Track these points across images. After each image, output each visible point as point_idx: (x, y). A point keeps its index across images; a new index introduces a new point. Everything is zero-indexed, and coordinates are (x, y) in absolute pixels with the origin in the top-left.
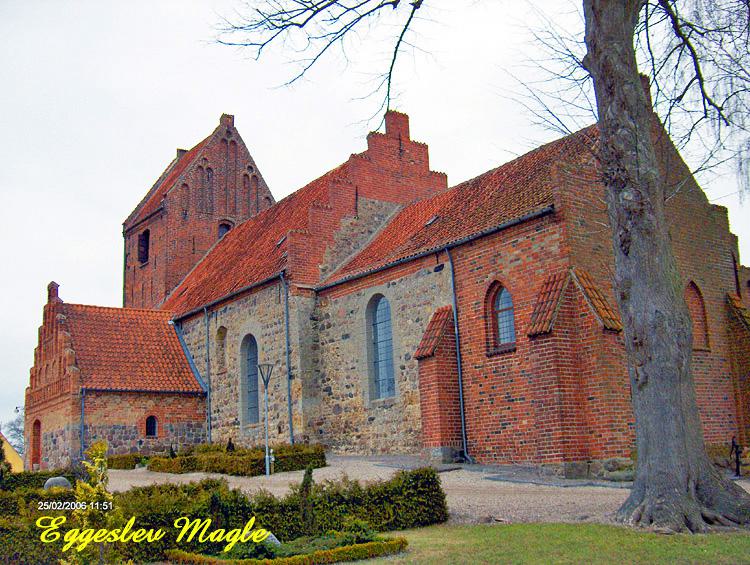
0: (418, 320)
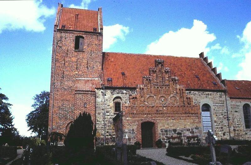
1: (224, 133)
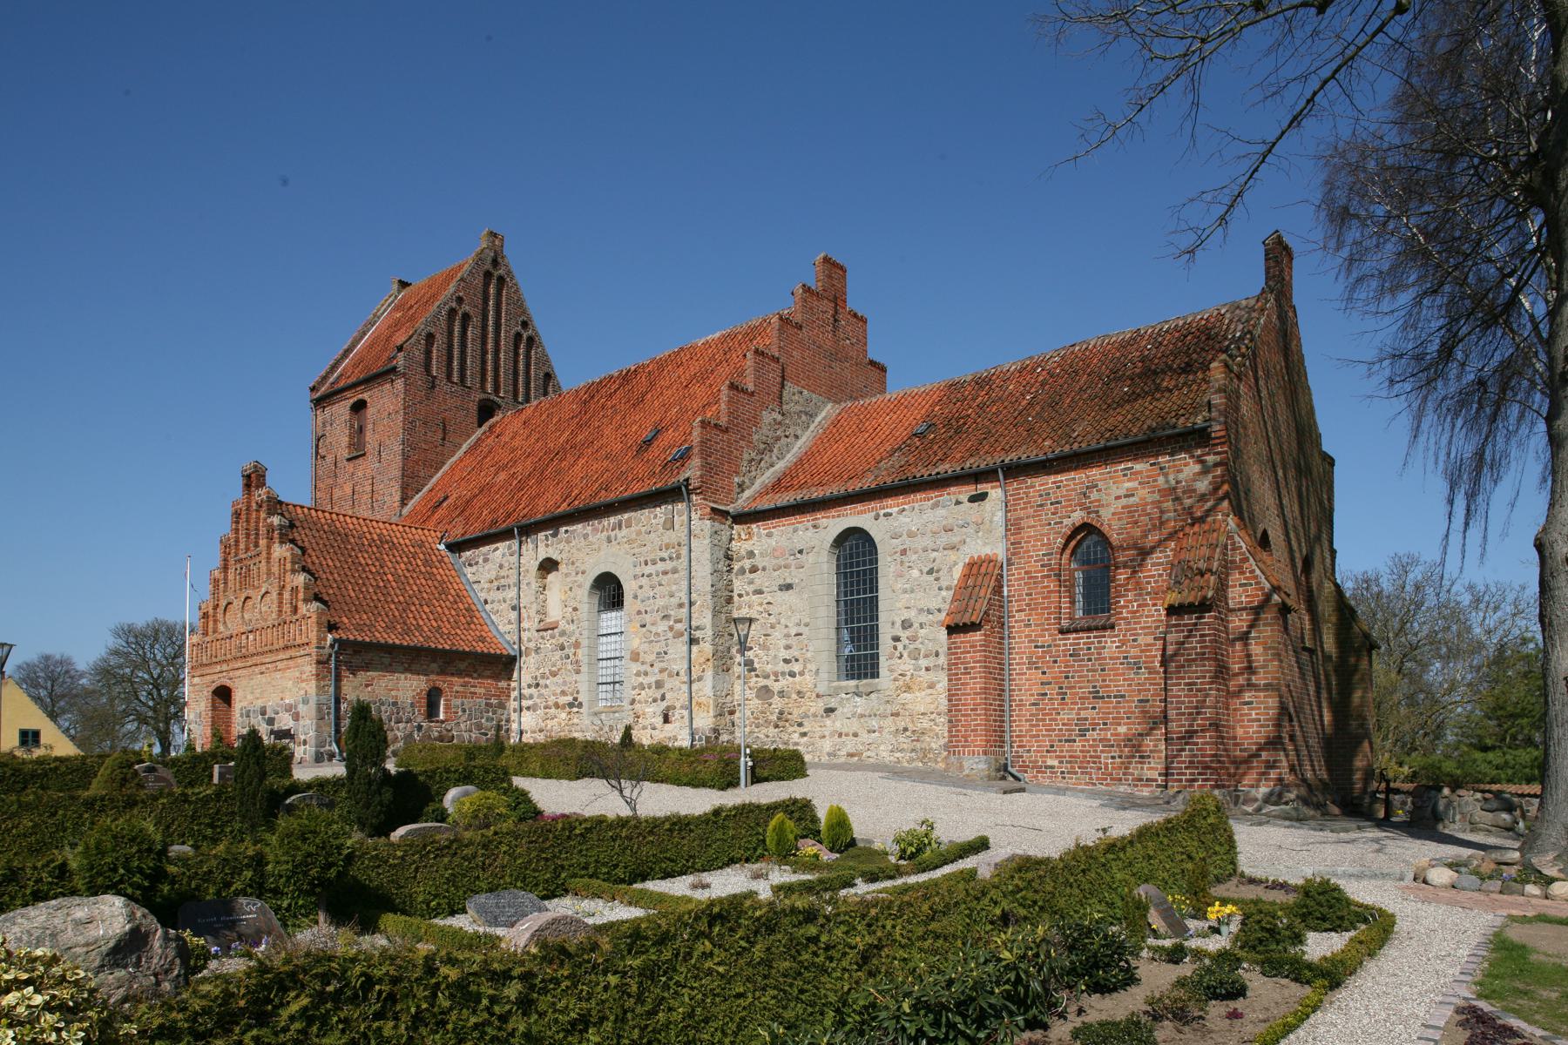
0: (930, 572)
1: (668, 708)
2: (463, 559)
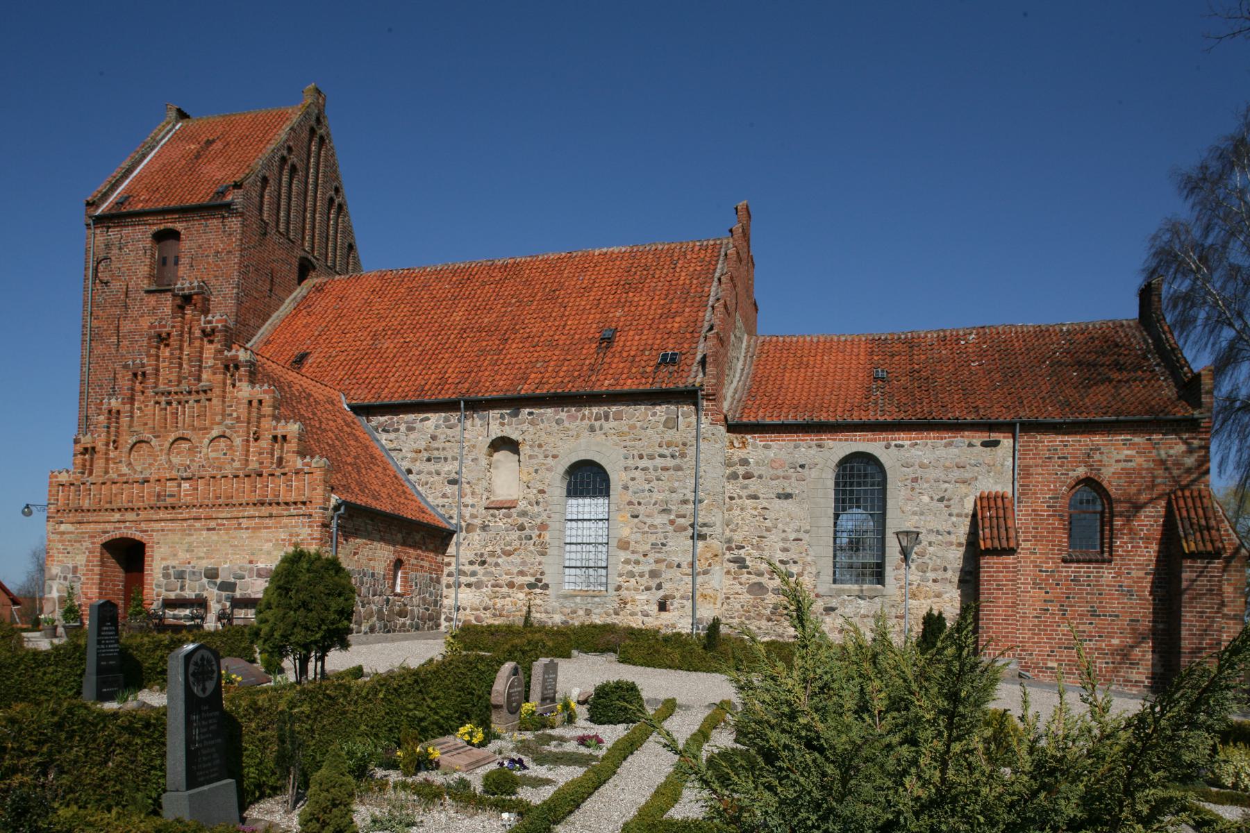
0: (941, 500)
1: (665, 598)
2: (374, 424)
